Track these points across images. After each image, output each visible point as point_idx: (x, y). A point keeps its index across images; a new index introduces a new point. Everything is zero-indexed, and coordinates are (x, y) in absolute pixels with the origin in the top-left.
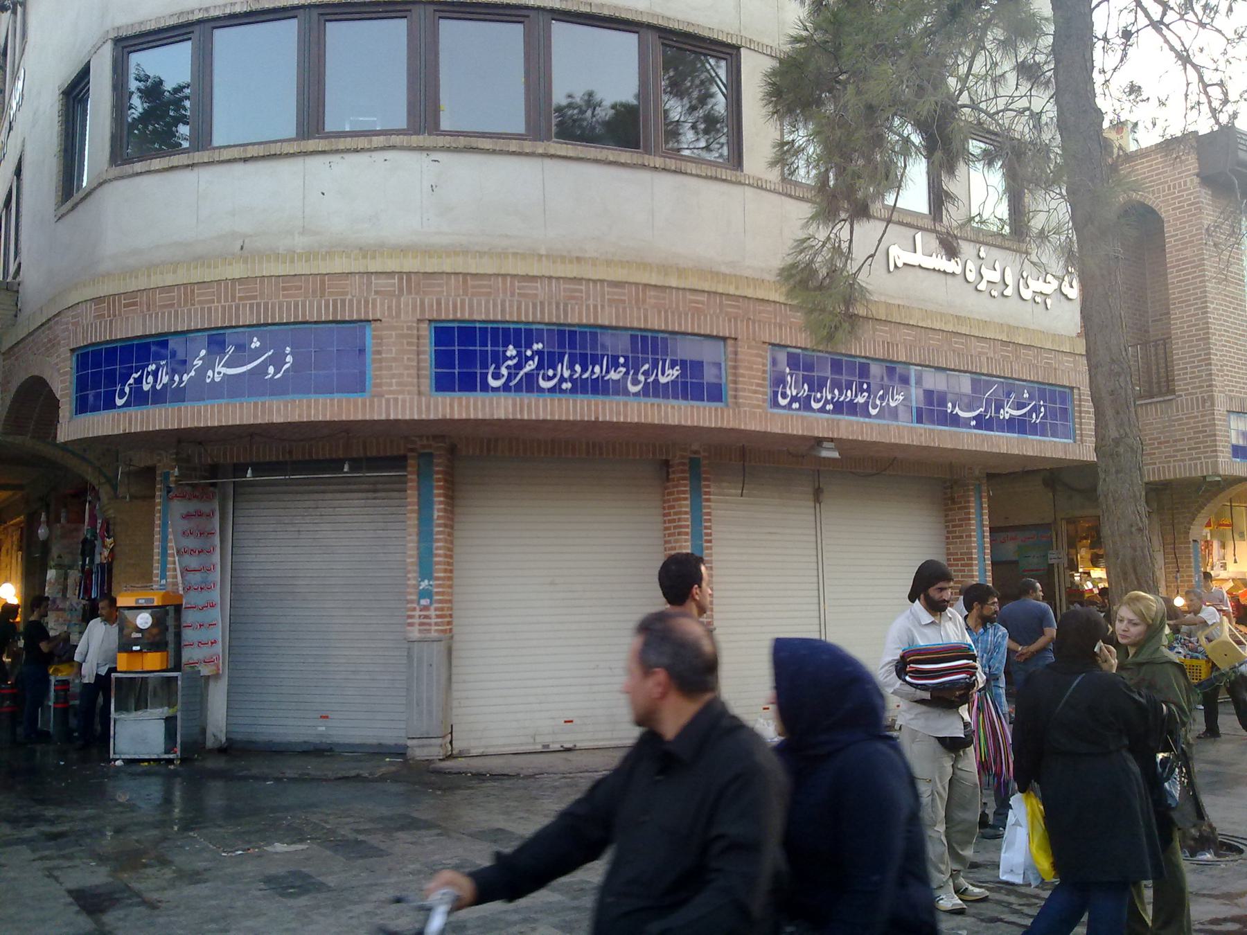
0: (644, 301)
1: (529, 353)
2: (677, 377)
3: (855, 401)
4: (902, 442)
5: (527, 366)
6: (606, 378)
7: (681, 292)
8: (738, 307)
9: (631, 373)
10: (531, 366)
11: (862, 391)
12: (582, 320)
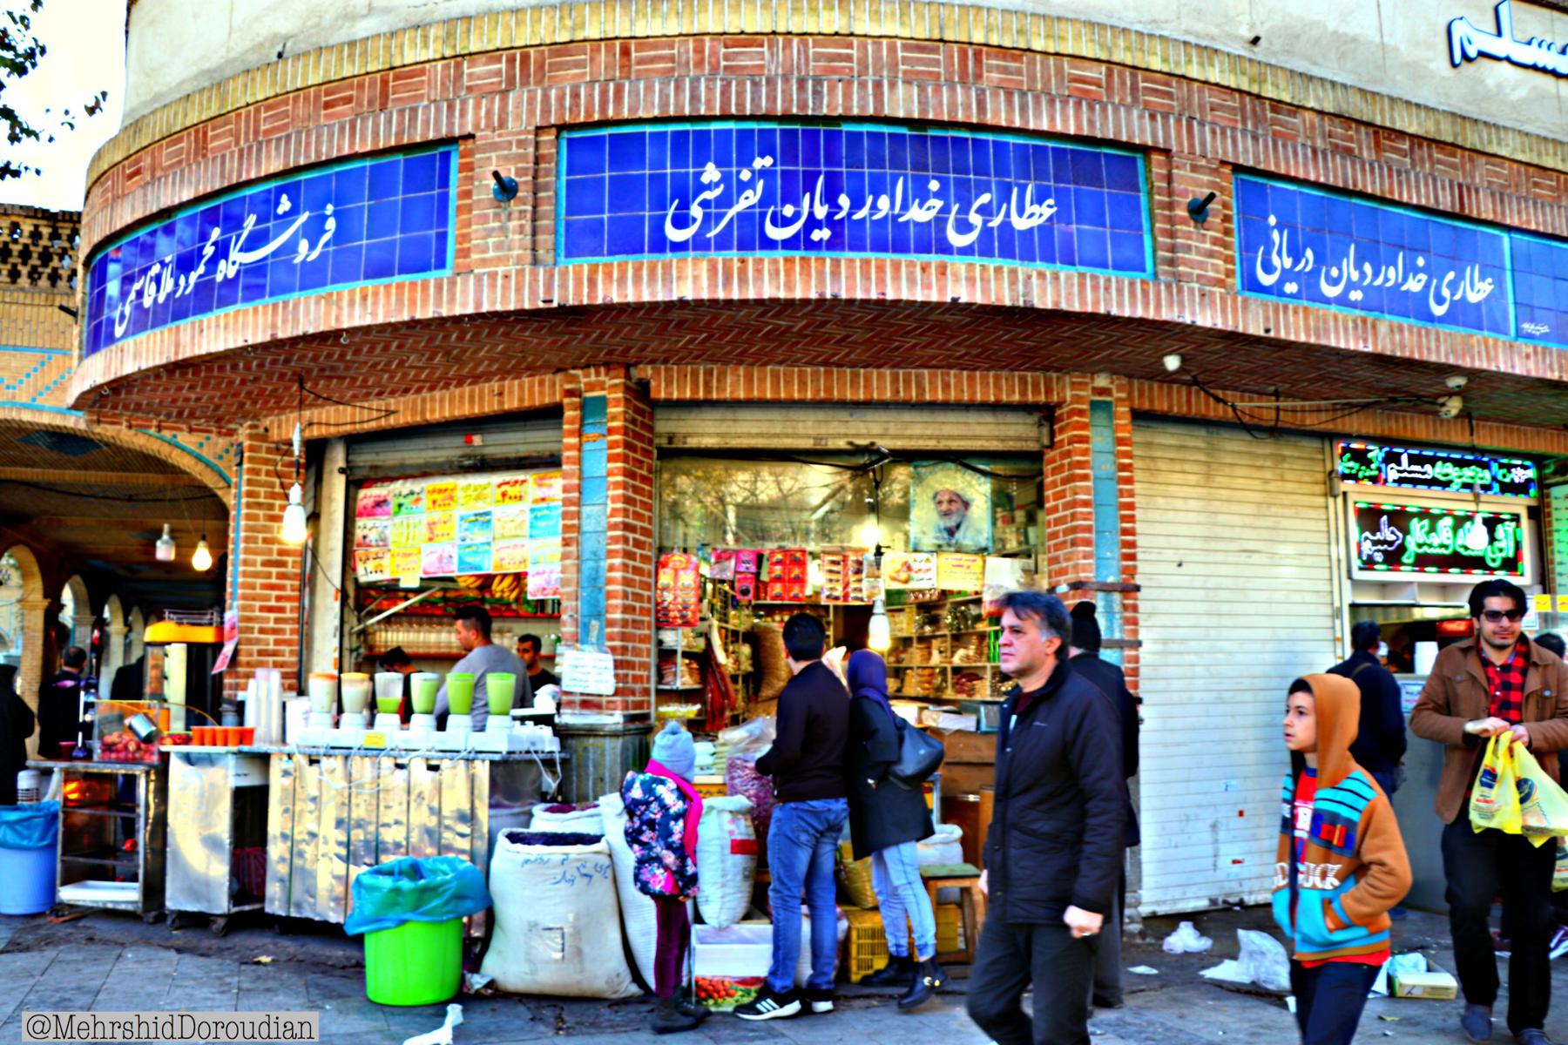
0: (978, 76)
1: (745, 175)
2: (1050, 219)
3: (1404, 288)
4: (1493, 368)
5: (742, 198)
6: (901, 220)
7: (1052, 60)
8: (1169, 95)
9: (955, 208)
10: (750, 199)
11: (1416, 271)
12: (851, 108)
